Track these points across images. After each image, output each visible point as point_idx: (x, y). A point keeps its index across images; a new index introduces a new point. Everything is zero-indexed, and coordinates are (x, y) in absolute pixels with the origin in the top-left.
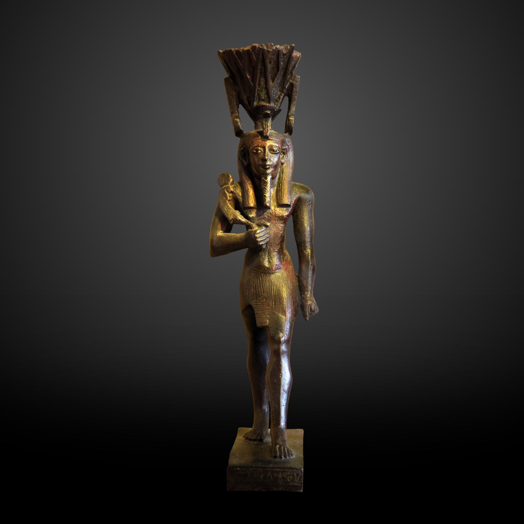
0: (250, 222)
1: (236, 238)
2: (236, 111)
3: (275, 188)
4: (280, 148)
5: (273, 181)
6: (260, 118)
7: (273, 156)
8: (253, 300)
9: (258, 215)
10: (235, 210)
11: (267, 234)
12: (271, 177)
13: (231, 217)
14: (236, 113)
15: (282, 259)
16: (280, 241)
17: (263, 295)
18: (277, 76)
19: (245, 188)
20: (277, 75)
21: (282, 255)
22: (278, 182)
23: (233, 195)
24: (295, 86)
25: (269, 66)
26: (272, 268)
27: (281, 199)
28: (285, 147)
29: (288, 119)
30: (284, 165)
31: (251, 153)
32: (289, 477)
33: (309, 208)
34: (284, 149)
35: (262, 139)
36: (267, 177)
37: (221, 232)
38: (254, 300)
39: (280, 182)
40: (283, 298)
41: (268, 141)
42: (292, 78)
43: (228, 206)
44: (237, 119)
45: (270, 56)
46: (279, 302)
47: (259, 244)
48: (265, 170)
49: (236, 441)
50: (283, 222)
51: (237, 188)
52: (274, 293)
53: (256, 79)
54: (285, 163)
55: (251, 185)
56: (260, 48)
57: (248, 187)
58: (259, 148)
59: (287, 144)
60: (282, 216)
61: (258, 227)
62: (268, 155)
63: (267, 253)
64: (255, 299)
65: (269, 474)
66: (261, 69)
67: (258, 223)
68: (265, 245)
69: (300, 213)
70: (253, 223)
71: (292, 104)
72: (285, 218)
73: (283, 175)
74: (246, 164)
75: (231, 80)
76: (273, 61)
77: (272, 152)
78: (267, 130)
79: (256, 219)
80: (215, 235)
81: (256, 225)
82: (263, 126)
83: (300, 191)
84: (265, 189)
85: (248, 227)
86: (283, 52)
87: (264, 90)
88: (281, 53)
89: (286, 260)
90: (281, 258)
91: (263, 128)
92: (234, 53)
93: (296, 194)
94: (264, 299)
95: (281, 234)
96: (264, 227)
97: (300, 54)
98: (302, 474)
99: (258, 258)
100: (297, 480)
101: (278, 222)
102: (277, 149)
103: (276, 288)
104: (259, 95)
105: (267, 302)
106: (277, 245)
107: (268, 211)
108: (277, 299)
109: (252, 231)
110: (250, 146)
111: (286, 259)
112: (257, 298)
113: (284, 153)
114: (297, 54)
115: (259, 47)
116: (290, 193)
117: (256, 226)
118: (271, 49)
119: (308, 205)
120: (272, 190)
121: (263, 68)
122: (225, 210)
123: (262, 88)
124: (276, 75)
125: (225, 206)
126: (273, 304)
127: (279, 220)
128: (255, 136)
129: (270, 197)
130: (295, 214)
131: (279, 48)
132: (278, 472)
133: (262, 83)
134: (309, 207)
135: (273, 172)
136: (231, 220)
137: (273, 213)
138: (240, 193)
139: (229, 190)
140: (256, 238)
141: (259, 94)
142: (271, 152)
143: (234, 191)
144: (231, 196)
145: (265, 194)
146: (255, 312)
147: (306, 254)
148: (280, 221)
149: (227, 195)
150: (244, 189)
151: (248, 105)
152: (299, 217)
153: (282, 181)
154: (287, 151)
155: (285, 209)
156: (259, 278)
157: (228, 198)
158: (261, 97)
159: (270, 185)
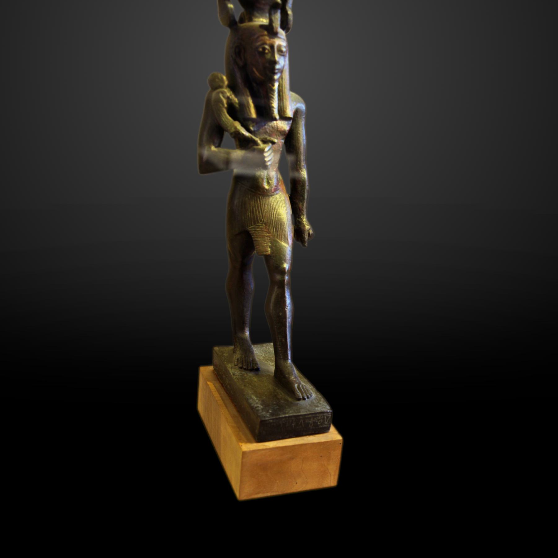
8: (250, 225)
17: (262, 220)
26: (271, 190)
38: (252, 225)
40: (285, 224)
46: (281, 229)
52: (275, 218)
60: (284, 131)
64: (253, 224)
65: (301, 421)
94: (264, 225)
98: (330, 415)
100: (326, 422)
103: (276, 213)
105: (267, 228)
108: (278, 226)
112: (255, 223)
126: (275, 231)
132: (310, 418)
146: (253, 239)
156: (257, 201)
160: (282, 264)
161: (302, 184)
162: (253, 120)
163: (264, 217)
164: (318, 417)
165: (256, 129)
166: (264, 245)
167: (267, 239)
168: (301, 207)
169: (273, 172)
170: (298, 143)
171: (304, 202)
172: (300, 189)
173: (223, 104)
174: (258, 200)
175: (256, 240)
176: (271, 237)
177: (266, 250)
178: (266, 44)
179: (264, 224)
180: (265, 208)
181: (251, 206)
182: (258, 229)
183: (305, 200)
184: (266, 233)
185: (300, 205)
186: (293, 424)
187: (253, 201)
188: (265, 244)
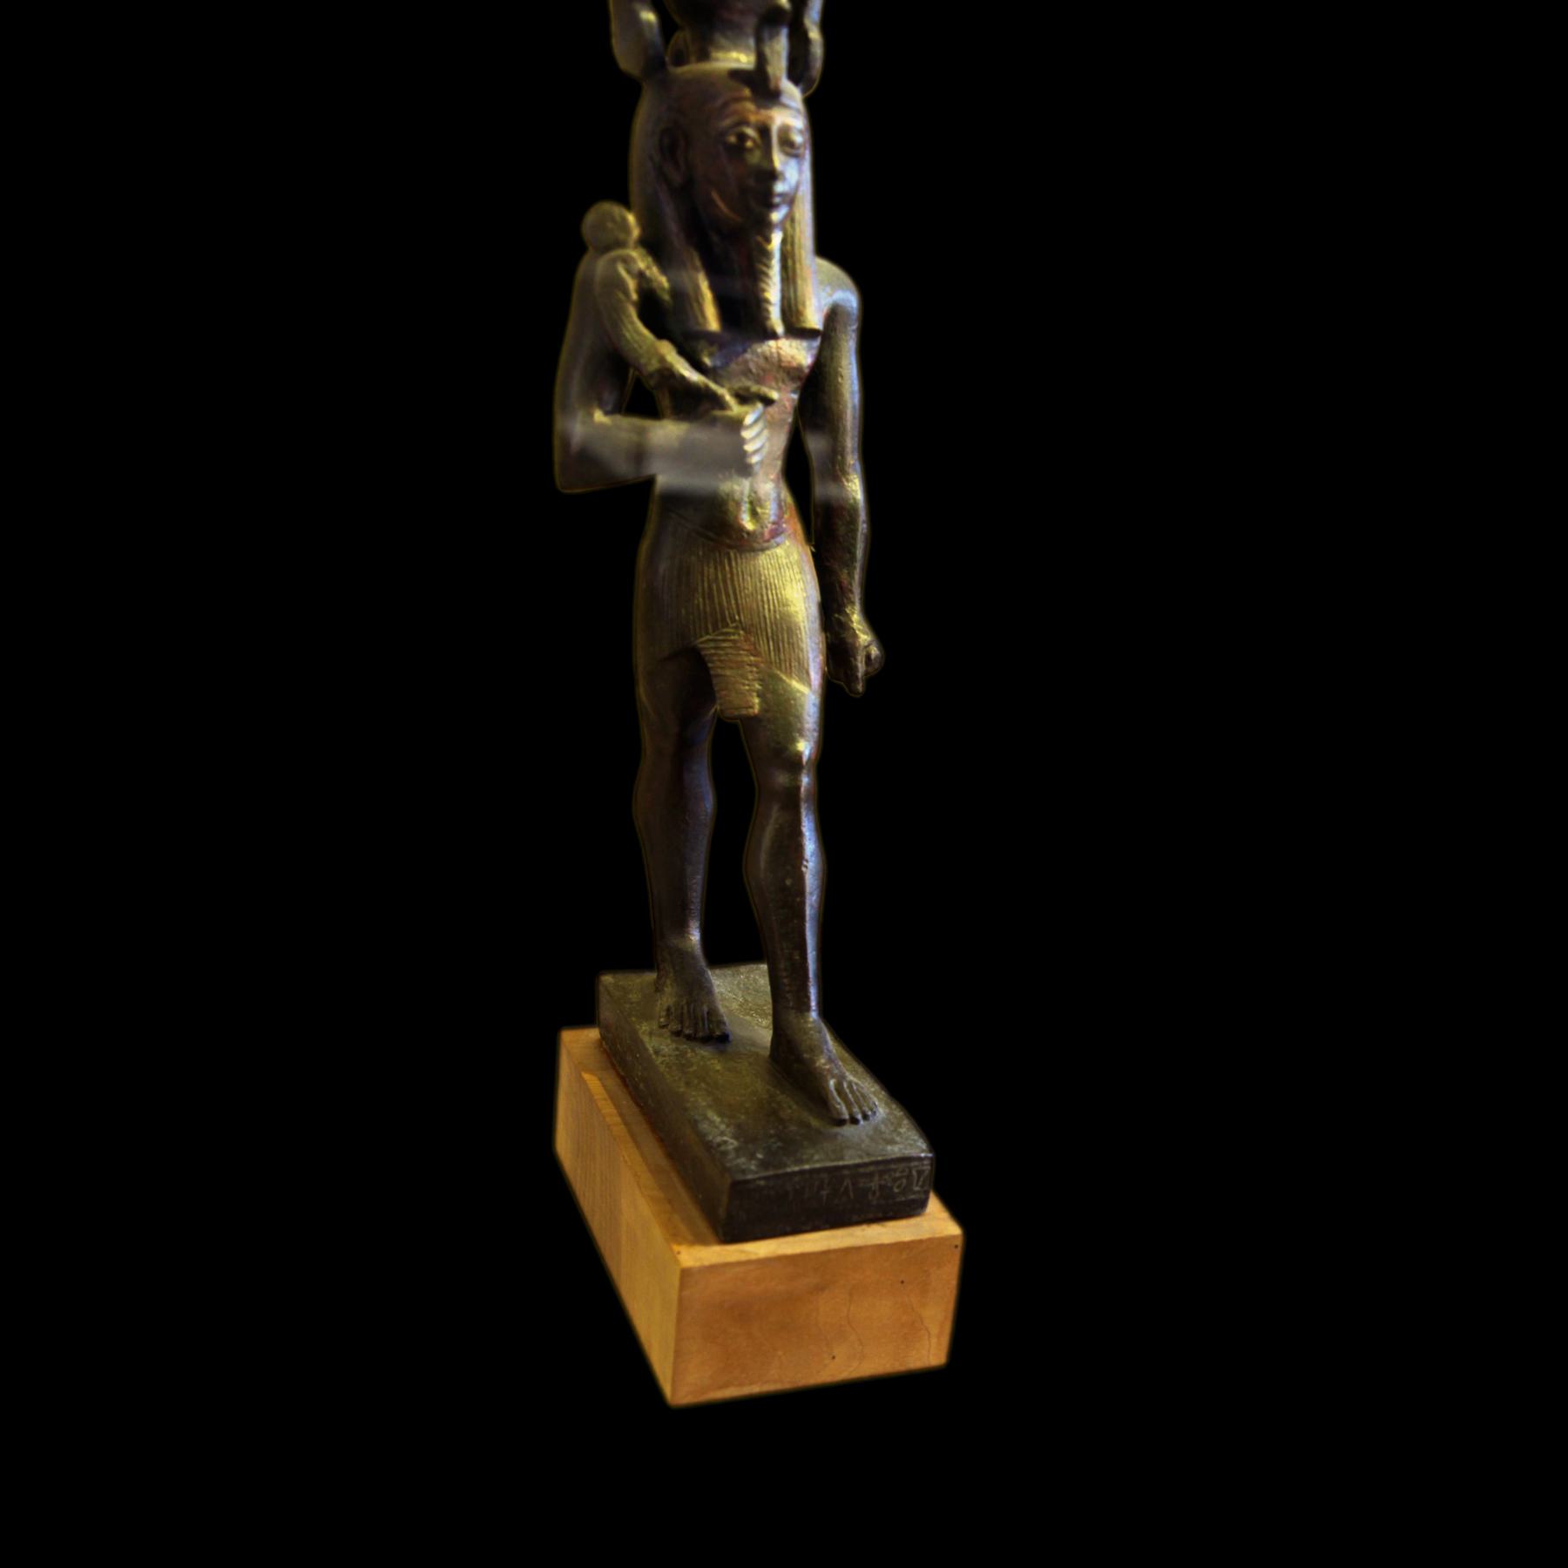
8: (703, 633)
17: (737, 617)
26: (762, 534)
32: (897, 1184)
38: (707, 633)
40: (800, 629)
46: (789, 643)
49: (953, 1282)
52: (772, 612)
60: (799, 368)
64: (711, 631)
65: (845, 1184)
94: (742, 632)
98: (927, 1167)
100: (917, 1185)
101: (783, 386)
103: (775, 597)
105: (750, 641)
108: (782, 634)
112: (715, 628)
126: (772, 648)
132: (871, 1175)
146: (712, 672)
156: (722, 564)
160: (794, 741)
161: (848, 518)
162: (710, 337)
163: (743, 609)
164: (895, 1170)
165: (718, 363)
166: (742, 688)
167: (751, 672)
168: (846, 582)
169: (766, 483)
170: (838, 402)
171: (855, 568)
172: (842, 530)
173: (626, 292)
174: (726, 561)
175: (718, 676)
176: (762, 665)
177: (747, 701)
178: (746, 123)
179: (743, 629)
180: (746, 585)
181: (706, 579)
182: (725, 645)
183: (856, 561)
184: (747, 656)
185: (844, 576)
186: (824, 1193)
187: (712, 565)
188: (744, 685)
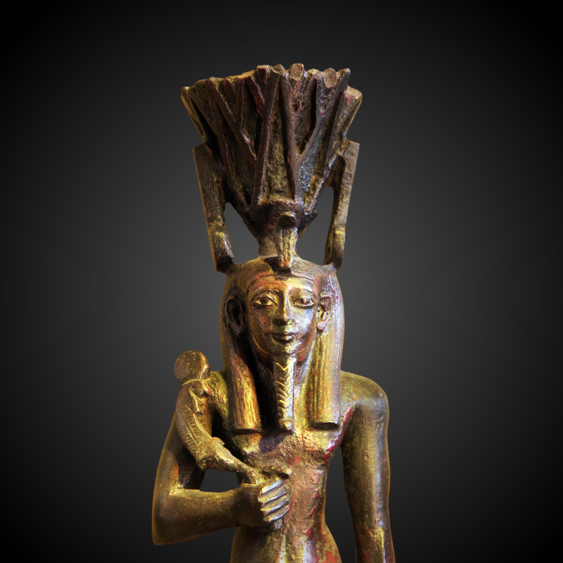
0: (245, 466)
1: (213, 503)
2: (219, 217)
3: (304, 385)
4: (317, 295)
5: (300, 370)
6: (271, 231)
7: (299, 314)
9: (265, 448)
10: (213, 436)
11: (285, 494)
12: (295, 360)
13: (201, 454)
14: (219, 220)
15: (318, 552)
16: (314, 510)
18: (311, 139)
19: (236, 385)
20: (310, 136)
21: (319, 542)
22: (311, 373)
23: (209, 402)
24: (347, 165)
25: (294, 117)
27: (318, 412)
28: (326, 294)
29: (332, 234)
30: (323, 334)
31: (250, 307)
33: (379, 431)
34: (325, 298)
35: (275, 276)
36: (286, 360)
37: (178, 488)
39: (315, 371)
41: (290, 279)
42: (342, 146)
43: (195, 426)
44: (221, 233)
45: (295, 93)
47: (265, 519)
48: (281, 345)
50: (323, 465)
51: (217, 384)
53: (264, 144)
54: (325, 330)
55: (248, 379)
56: (274, 74)
57: (242, 383)
58: (269, 296)
59: (330, 287)
60: (321, 452)
61: (265, 479)
62: (288, 311)
63: (284, 537)
66: (275, 122)
67: (264, 468)
68: (280, 521)
69: (360, 443)
70: (253, 466)
71: (341, 202)
72: (327, 455)
73: (321, 357)
74: (239, 332)
75: (210, 151)
76: (303, 104)
77: (298, 304)
78: (287, 256)
79: (260, 458)
80: (165, 494)
81: (260, 473)
82: (278, 246)
83: (360, 391)
84: (282, 388)
85: (243, 477)
86: (324, 84)
87: (280, 169)
88: (320, 86)
89: (328, 553)
90: (316, 549)
91: (279, 251)
92: (217, 89)
93: (350, 399)
95: (318, 492)
96: (277, 479)
97: (361, 94)
99: (263, 550)
101: (310, 464)
102: (309, 298)
104: (269, 179)
106: (308, 518)
107: (287, 438)
109: (251, 488)
110: (248, 292)
111: (327, 552)
113: (323, 308)
114: (353, 93)
115: (271, 71)
116: (338, 396)
117: (261, 475)
118: (299, 76)
119: (378, 423)
120: (297, 391)
121: (279, 121)
122: (188, 436)
123: (277, 165)
124: (307, 137)
125: (188, 426)
127: (312, 461)
128: (260, 269)
129: (293, 407)
130: (348, 445)
131: (316, 74)
133: (278, 154)
134: (379, 429)
135: (299, 350)
136: (202, 460)
137: (300, 444)
138: (225, 396)
139: (200, 389)
140: (260, 505)
141: (270, 177)
142: (296, 304)
143: (210, 392)
144: (204, 403)
145: (281, 401)
147: (375, 540)
148: (315, 462)
149: (194, 402)
150: (233, 389)
151: (246, 203)
152: (356, 451)
153: (319, 370)
154: (329, 304)
155: (326, 434)
157: (196, 409)
158: (275, 184)
159: (292, 381)
170: (365, 475)
